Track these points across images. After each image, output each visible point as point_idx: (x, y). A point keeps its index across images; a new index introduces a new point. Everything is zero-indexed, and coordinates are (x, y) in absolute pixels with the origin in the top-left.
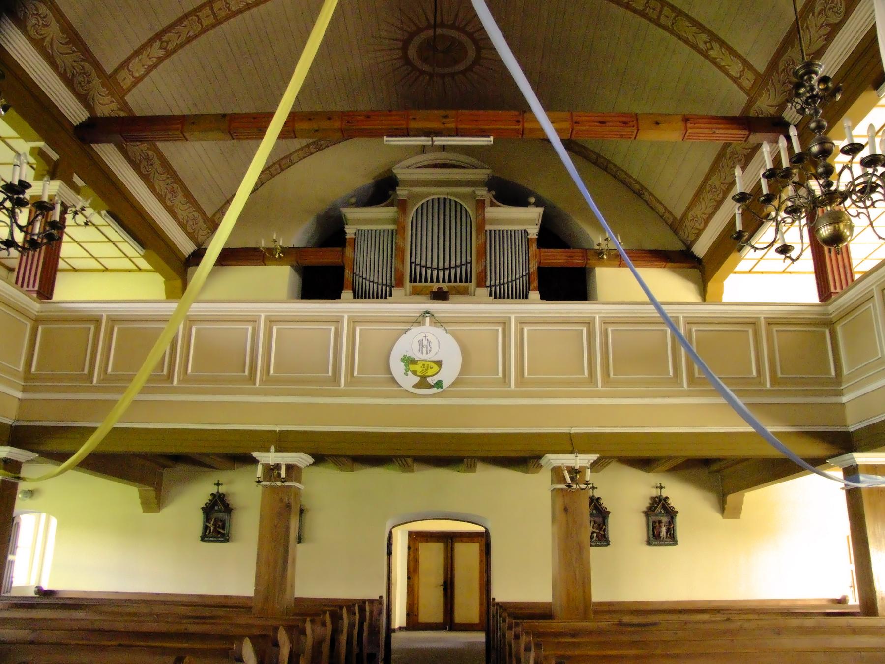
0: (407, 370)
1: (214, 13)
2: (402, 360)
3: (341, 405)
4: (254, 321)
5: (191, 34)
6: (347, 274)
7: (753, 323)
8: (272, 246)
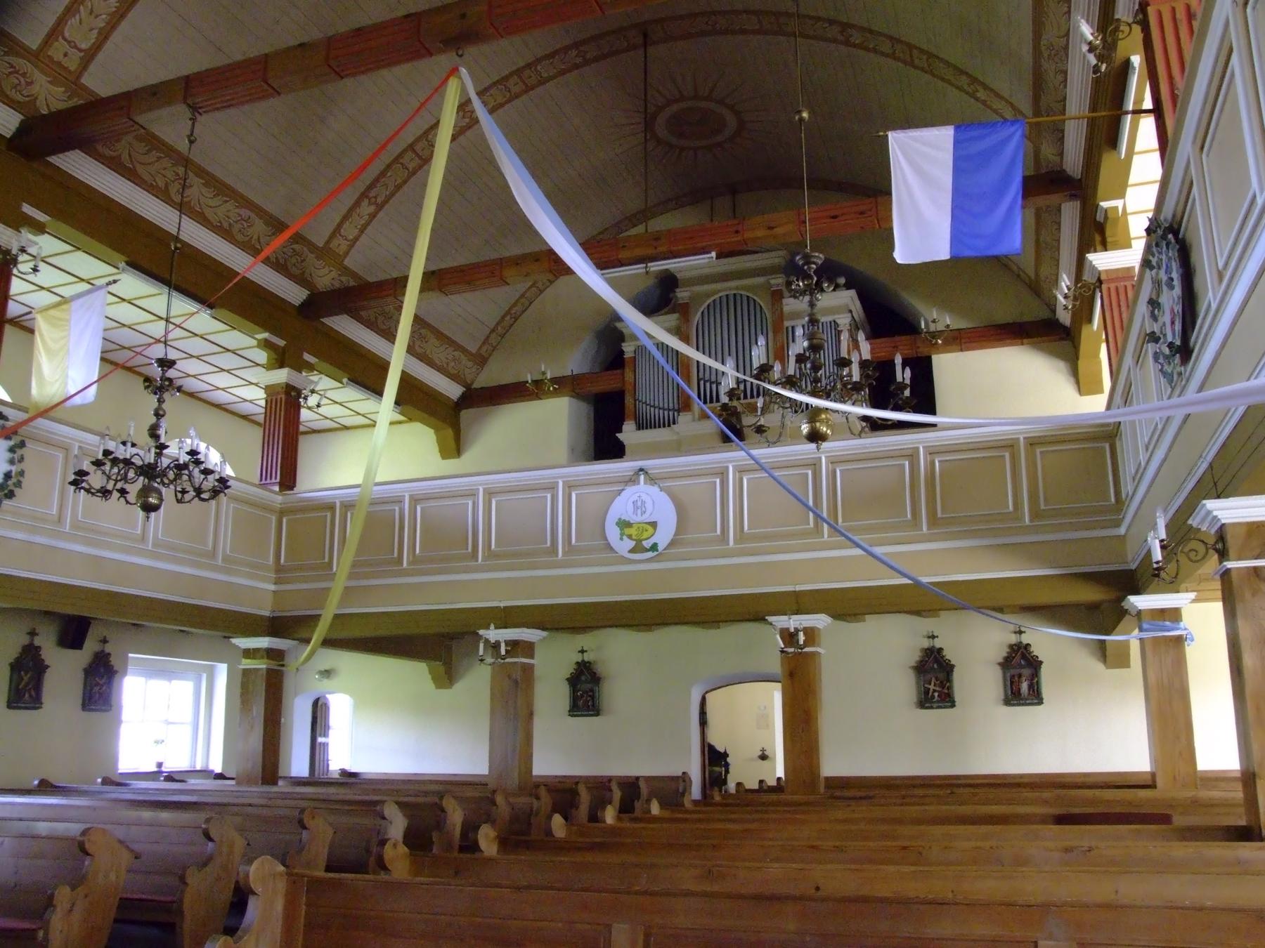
0: (622, 535)
1: (417, 155)
2: (617, 524)
3: (571, 575)
4: (473, 494)
5: (399, 181)
6: (629, 401)
7: (1010, 445)
8: (540, 377)
